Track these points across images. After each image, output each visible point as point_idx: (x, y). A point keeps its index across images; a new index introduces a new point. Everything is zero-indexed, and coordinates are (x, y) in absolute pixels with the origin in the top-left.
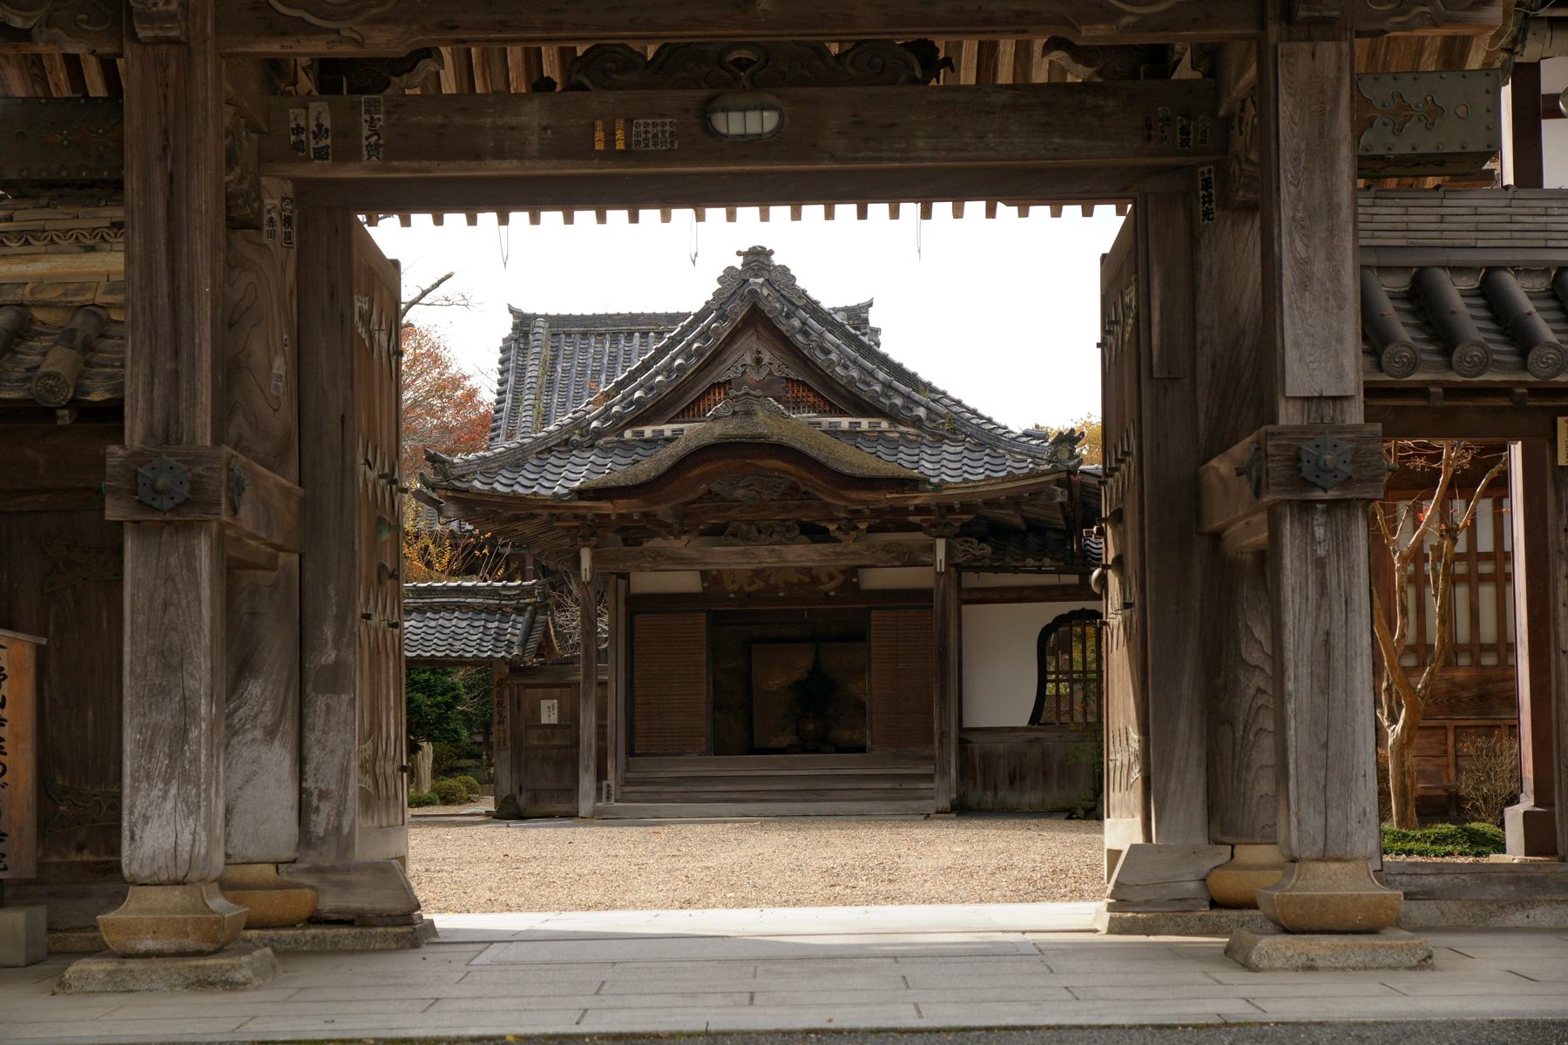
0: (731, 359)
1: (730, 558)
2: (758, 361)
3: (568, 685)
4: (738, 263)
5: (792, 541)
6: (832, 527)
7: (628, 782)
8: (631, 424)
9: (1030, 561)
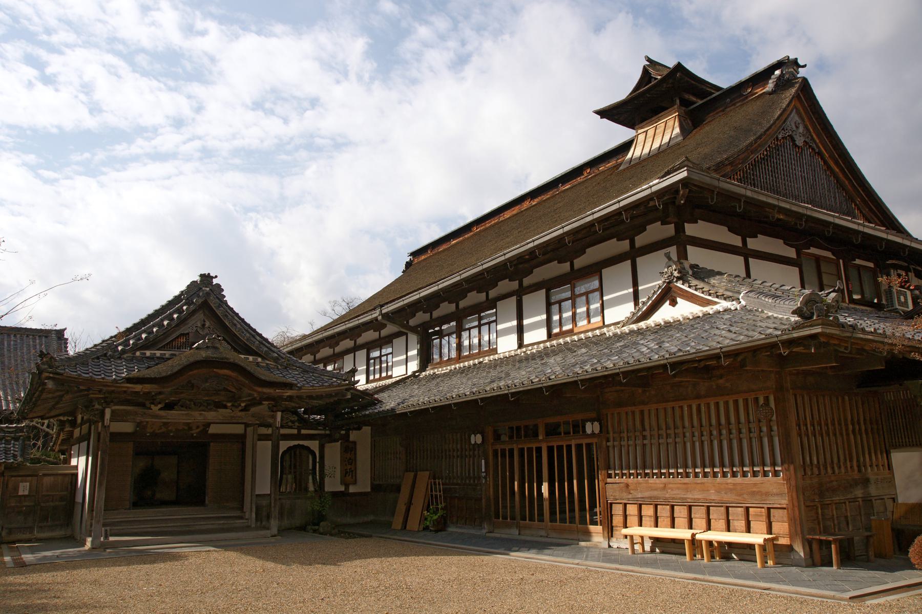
0: (191, 322)
2: (204, 325)
3: (36, 476)
5: (210, 410)
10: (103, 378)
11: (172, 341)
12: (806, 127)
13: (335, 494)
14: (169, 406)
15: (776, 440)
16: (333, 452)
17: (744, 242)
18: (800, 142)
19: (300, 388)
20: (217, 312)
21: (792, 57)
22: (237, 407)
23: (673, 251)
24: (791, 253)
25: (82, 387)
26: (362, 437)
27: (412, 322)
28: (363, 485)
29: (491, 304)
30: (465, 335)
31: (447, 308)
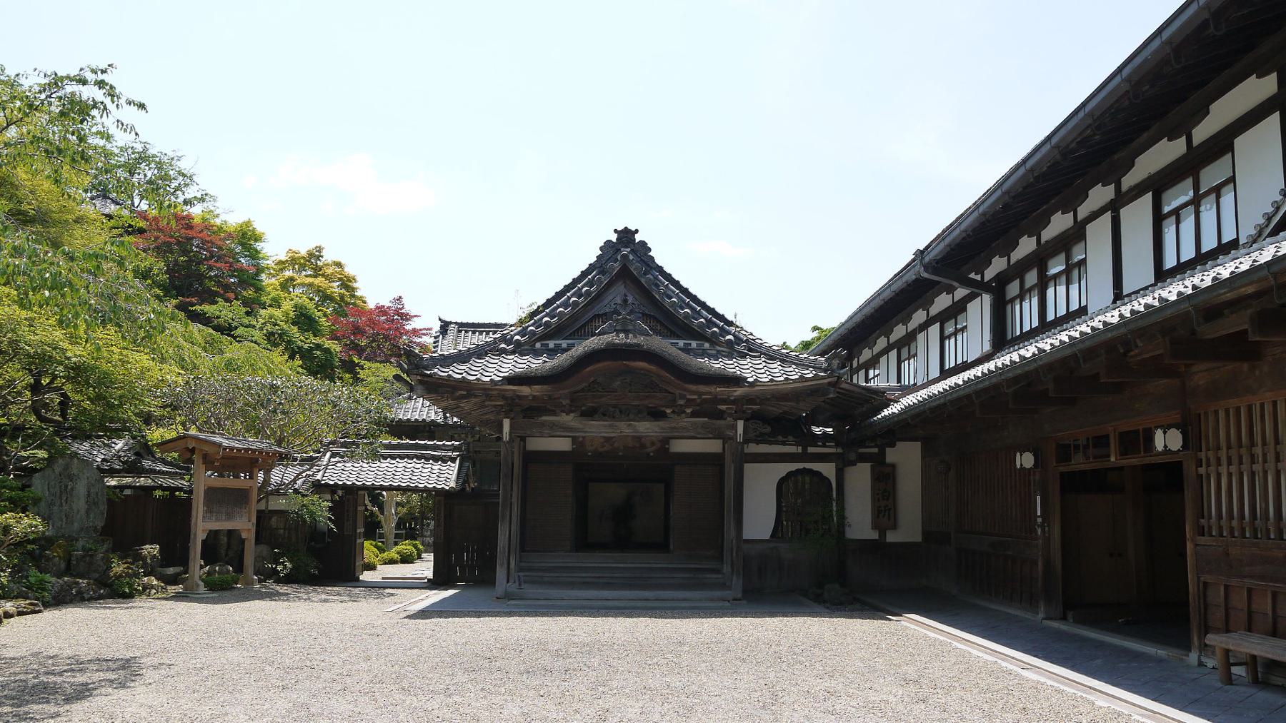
0: (608, 298)
1: (597, 430)
2: (625, 301)
4: (614, 238)
6: (669, 411)
7: (521, 570)
8: (540, 339)
9: (780, 438)
11: (584, 325)
13: (865, 545)
16: (860, 478)
19: (752, 384)
20: (643, 281)
28: (908, 530)
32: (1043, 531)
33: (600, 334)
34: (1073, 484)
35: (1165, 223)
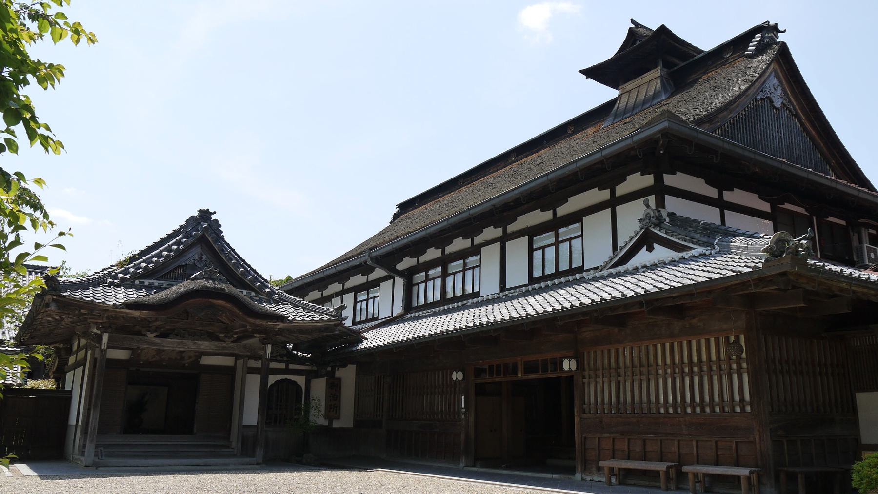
2: (201, 258)
5: (204, 340)
10: (103, 303)
12: (784, 89)
14: (164, 335)
15: (745, 377)
16: (319, 387)
17: (721, 195)
18: (778, 103)
19: (291, 322)
21: (772, 23)
22: (229, 338)
23: (652, 199)
24: (766, 207)
25: (82, 311)
26: (347, 375)
27: (400, 267)
28: (345, 421)
29: (476, 250)
30: (450, 280)
31: (433, 254)
32: (466, 416)
33: (192, 279)
34: (481, 391)
35: (535, 253)
